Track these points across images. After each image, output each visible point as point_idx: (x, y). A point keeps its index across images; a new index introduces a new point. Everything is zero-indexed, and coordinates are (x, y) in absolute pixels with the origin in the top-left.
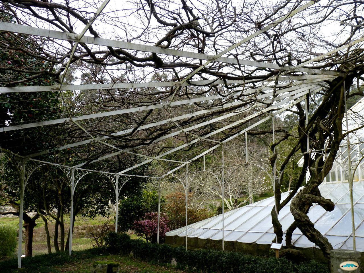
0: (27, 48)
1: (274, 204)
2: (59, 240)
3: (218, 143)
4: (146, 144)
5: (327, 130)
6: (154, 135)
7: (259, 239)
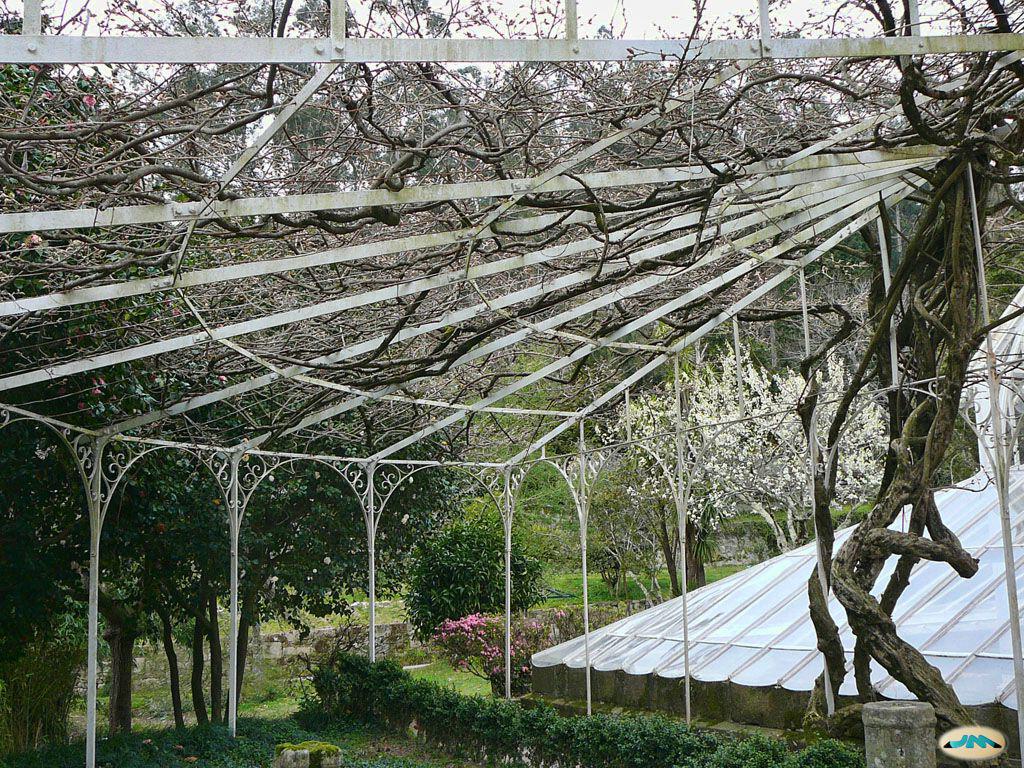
0: (97, 106)
1: (816, 560)
2: (207, 689)
3: (661, 353)
4: (431, 374)
5: (935, 319)
6: (450, 348)
7: (741, 669)
